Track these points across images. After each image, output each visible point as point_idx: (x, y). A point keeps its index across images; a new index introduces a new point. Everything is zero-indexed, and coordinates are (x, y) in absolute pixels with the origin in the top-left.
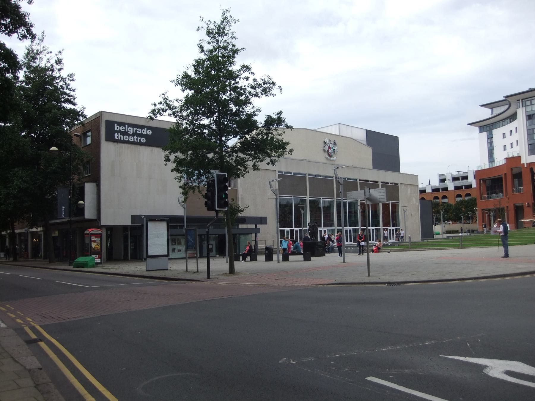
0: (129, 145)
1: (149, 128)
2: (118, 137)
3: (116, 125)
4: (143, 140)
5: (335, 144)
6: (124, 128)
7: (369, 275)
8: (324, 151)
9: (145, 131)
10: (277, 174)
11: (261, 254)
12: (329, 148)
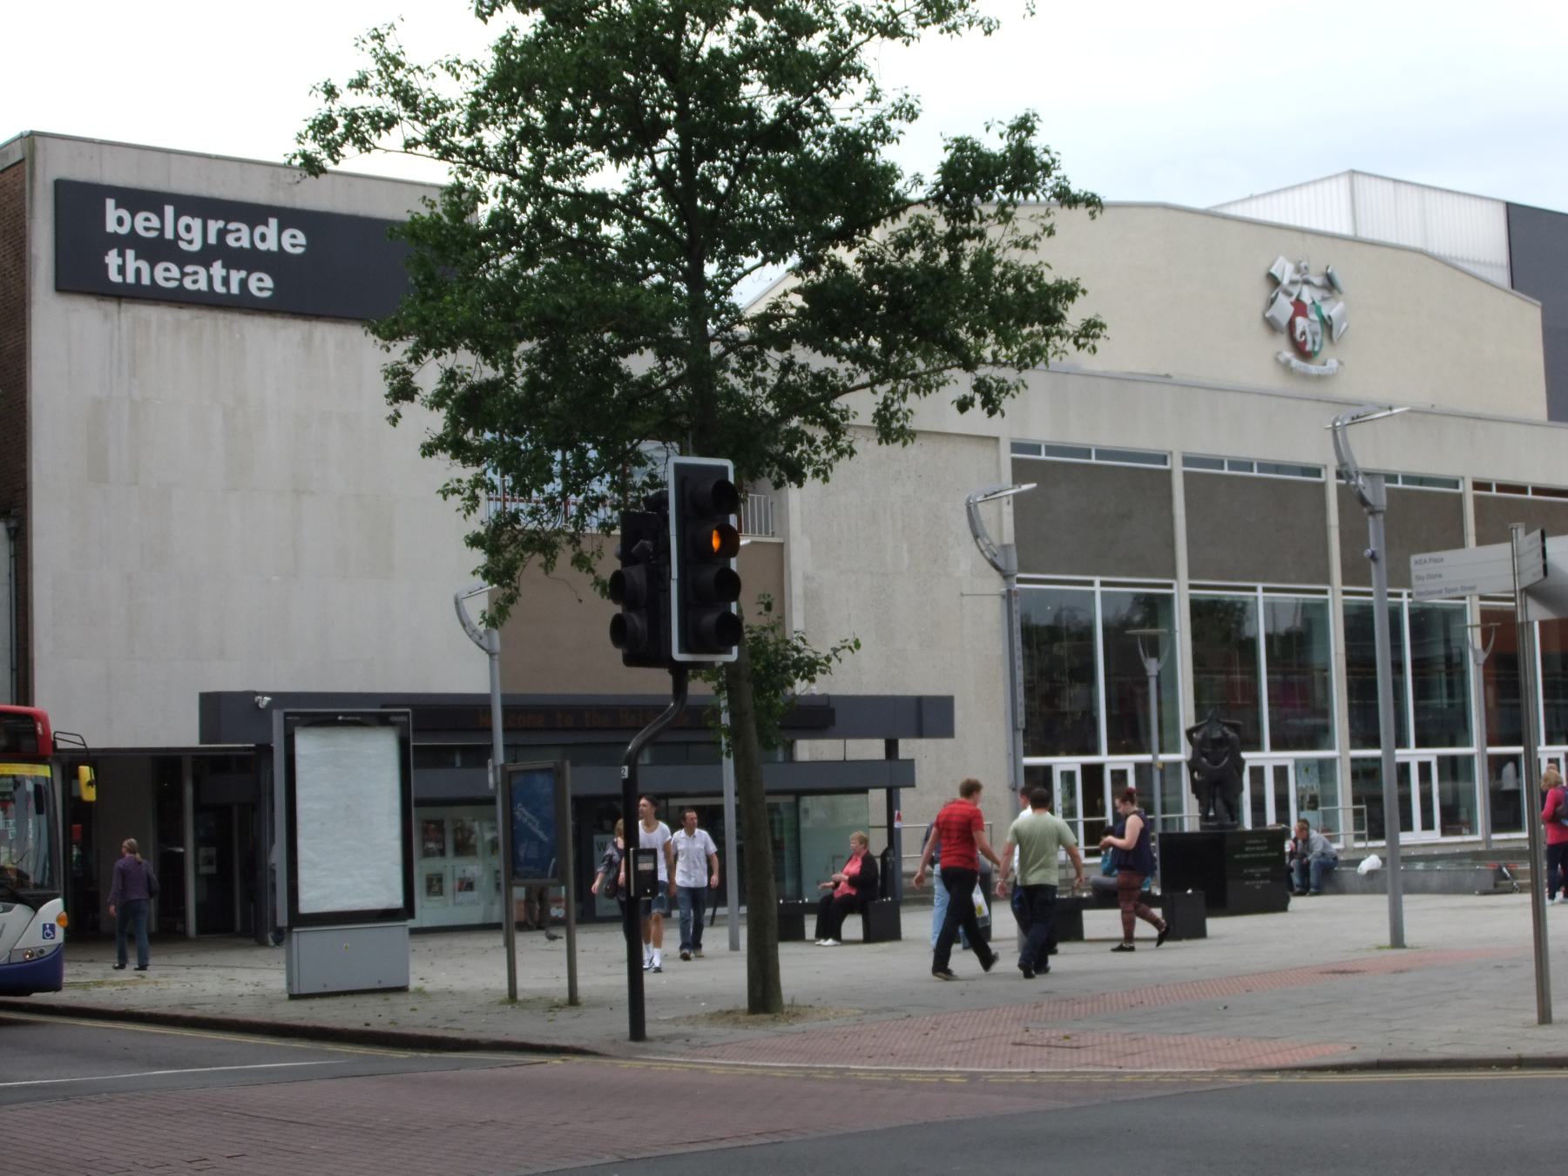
0: (186, 315)
1: (289, 218)
2: (122, 270)
4: (261, 284)
5: (1330, 284)
6: (155, 222)
7: (1545, 1017)
8: (1271, 325)
9: (270, 237)
10: (1007, 456)
12: (1300, 308)
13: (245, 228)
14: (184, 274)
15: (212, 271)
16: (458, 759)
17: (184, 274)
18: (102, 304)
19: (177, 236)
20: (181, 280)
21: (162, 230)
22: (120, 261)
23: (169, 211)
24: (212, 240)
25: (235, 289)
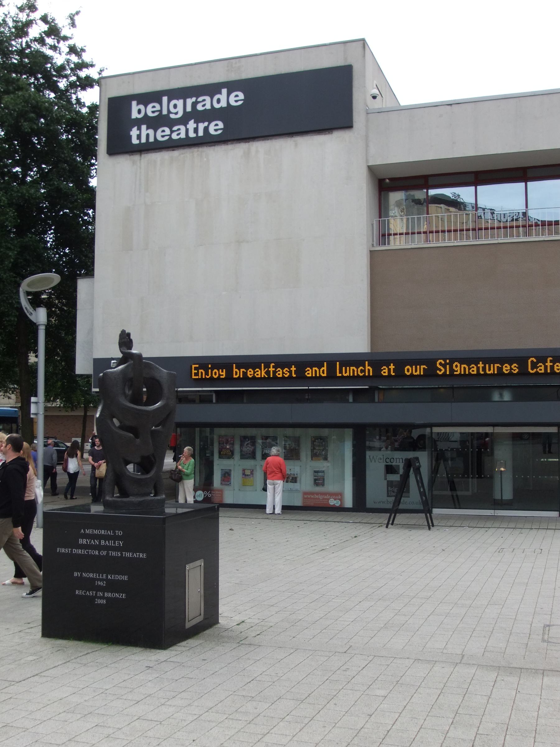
0: (176, 153)
1: (232, 86)
2: (139, 137)
3: (134, 103)
4: (216, 127)
6: (158, 107)
9: (223, 100)
11: (83, 489)
13: (208, 99)
14: (172, 132)
15: (188, 126)
16: (351, 399)
17: (172, 132)
18: (132, 156)
19: (169, 112)
20: (170, 135)
21: (161, 111)
22: (138, 132)
23: (165, 99)
24: (189, 109)
25: (201, 133)
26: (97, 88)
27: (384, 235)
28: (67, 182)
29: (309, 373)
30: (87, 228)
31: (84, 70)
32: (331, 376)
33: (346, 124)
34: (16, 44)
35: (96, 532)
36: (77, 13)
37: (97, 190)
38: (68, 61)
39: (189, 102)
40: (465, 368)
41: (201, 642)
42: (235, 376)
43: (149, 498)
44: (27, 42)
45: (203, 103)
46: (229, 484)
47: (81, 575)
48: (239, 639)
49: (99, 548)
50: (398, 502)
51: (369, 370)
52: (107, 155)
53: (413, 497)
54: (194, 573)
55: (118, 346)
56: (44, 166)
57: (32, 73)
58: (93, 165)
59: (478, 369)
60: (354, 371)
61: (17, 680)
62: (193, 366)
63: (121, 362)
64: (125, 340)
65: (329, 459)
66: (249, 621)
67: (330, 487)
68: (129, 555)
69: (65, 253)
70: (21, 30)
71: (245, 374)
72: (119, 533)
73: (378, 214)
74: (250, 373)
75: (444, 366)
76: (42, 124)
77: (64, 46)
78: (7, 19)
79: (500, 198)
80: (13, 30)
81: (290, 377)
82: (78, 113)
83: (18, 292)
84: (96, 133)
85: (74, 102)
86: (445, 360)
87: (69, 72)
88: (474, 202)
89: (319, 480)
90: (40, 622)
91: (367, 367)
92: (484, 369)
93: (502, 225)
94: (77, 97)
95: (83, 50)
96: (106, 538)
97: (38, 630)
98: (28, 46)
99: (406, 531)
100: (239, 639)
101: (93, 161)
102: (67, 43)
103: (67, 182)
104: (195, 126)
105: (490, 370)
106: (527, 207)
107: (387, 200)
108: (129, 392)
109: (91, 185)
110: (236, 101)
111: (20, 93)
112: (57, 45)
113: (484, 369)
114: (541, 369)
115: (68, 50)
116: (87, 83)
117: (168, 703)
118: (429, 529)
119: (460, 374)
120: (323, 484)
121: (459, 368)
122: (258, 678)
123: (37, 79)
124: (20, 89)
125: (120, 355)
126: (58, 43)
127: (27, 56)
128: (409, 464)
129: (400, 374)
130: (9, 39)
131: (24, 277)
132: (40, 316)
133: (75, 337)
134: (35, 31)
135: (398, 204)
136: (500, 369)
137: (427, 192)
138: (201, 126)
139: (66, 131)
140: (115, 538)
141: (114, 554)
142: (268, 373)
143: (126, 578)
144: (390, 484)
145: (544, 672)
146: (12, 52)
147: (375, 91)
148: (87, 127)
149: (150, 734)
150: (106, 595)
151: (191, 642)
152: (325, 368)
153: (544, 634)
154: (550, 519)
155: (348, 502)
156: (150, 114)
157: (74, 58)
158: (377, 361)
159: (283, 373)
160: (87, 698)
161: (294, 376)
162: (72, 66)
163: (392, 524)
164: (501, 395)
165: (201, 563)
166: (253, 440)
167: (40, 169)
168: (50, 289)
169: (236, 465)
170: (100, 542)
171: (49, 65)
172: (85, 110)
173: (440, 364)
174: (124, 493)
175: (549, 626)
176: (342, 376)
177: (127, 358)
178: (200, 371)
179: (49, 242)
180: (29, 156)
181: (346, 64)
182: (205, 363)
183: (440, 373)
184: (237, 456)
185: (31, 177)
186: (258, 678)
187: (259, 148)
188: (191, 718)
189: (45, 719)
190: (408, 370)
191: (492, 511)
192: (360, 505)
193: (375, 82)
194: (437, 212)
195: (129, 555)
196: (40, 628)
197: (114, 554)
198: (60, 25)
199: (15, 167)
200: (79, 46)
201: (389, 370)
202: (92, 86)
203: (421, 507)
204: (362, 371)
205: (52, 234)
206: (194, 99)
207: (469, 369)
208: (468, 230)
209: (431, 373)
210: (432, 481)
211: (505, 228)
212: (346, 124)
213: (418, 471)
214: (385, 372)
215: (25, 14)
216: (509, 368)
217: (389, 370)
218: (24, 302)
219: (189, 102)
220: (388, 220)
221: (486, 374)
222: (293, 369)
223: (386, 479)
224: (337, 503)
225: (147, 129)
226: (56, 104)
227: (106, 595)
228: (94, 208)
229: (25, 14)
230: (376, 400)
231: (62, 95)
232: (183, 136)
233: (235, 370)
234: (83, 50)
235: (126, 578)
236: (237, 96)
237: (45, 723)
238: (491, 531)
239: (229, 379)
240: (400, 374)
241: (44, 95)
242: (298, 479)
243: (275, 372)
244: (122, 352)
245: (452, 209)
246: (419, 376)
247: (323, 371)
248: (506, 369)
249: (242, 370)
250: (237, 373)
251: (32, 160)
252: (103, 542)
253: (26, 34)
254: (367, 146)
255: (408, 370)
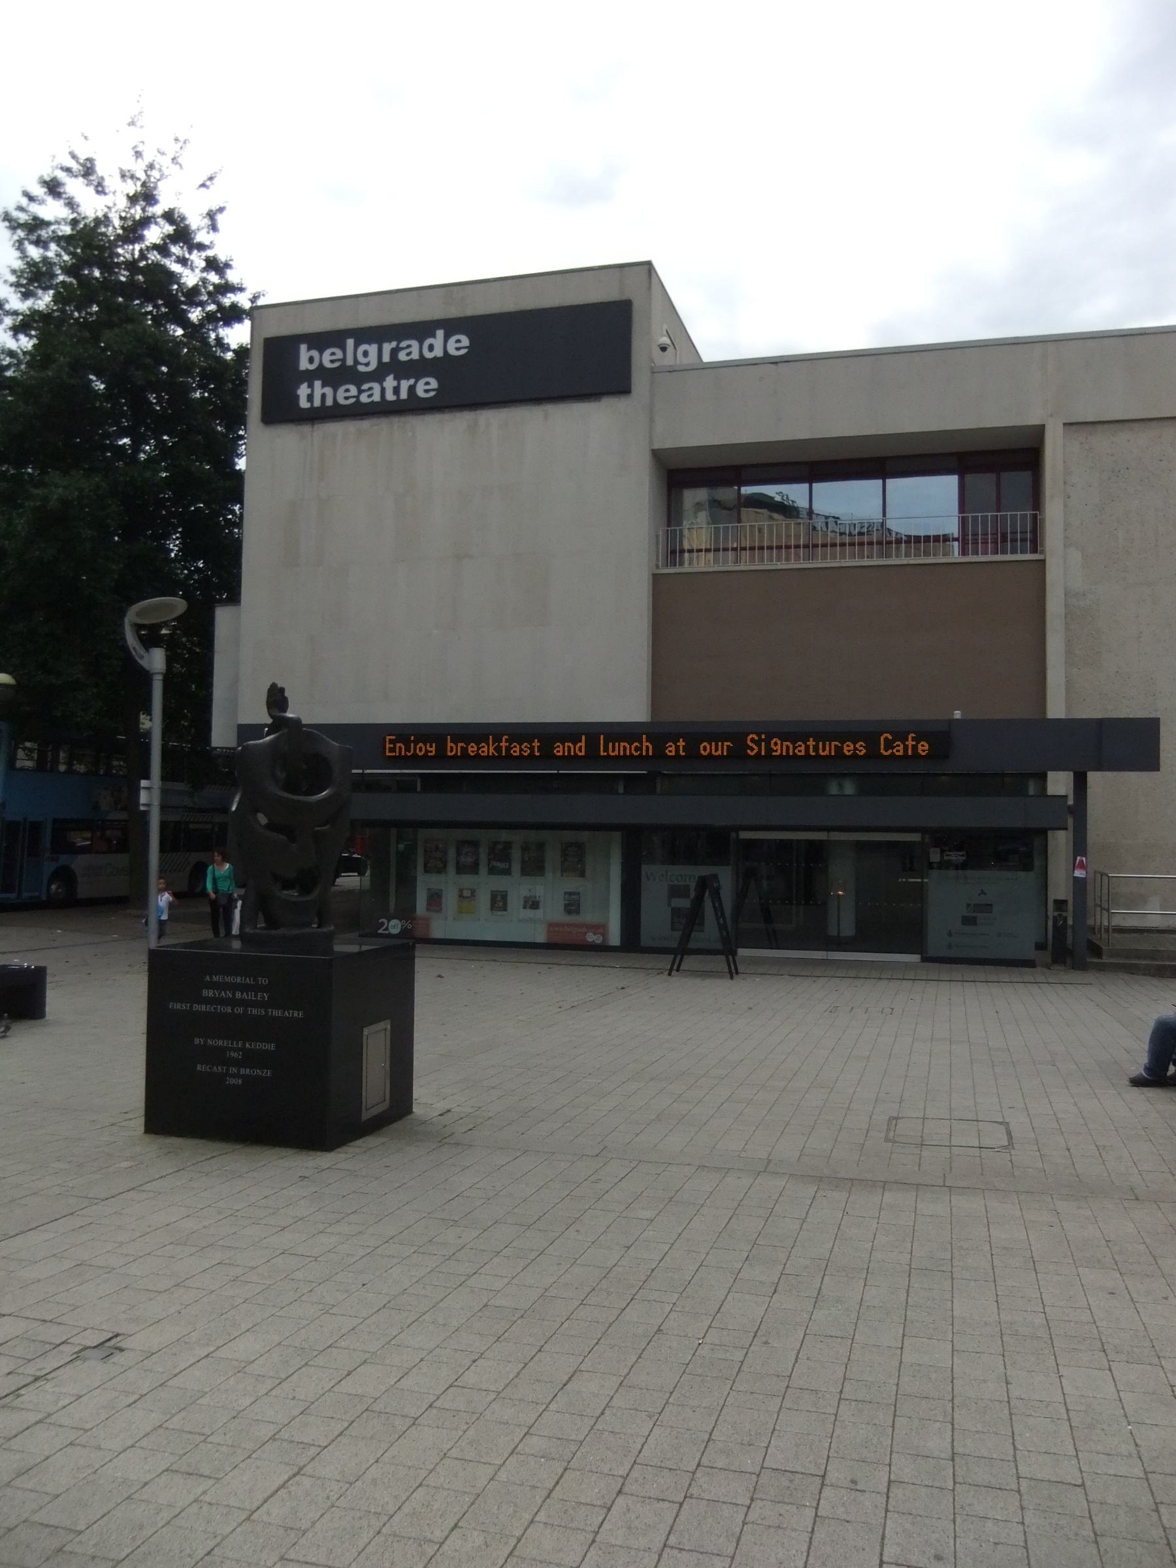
0: (366, 424)
1: (451, 326)
2: (310, 398)
3: (303, 348)
4: (426, 387)
6: (339, 354)
9: (437, 346)
13: (415, 344)
14: (360, 392)
15: (385, 384)
17: (360, 392)
19: (356, 362)
20: (357, 397)
21: (344, 360)
22: (309, 391)
23: (350, 343)
24: (386, 358)
25: (404, 395)
26: (247, 323)
27: (673, 552)
28: (201, 463)
29: (559, 750)
30: (231, 532)
31: (229, 295)
32: (592, 755)
33: (624, 389)
34: (124, 252)
35: (228, 979)
36: (221, 210)
37: (246, 477)
38: (204, 281)
39: (387, 347)
40: (788, 747)
41: (384, 1140)
42: (449, 754)
43: (307, 930)
44: (141, 251)
45: (408, 351)
46: (440, 911)
47: (205, 1042)
48: (443, 1137)
49: (233, 1003)
50: (686, 938)
51: (647, 747)
52: (261, 424)
53: (710, 931)
54: (376, 1042)
55: (266, 709)
56: (165, 438)
57: (149, 298)
58: (242, 437)
59: (807, 747)
60: (625, 748)
61: (102, 1196)
62: (388, 738)
63: (273, 728)
64: (277, 698)
65: (588, 873)
66: (457, 1109)
67: (588, 916)
68: (277, 1013)
69: (197, 568)
70: (133, 231)
71: (464, 750)
72: (263, 981)
73: (665, 519)
74: (472, 749)
75: (758, 743)
76: (163, 373)
77: (197, 259)
78: (110, 215)
79: (847, 501)
80: (120, 232)
81: (532, 755)
82: (221, 360)
83: (122, 625)
84: (245, 392)
85: (213, 343)
86: (759, 735)
87: (205, 298)
88: (807, 506)
89: (572, 905)
90: (142, 1112)
91: (645, 744)
92: (816, 748)
93: (847, 539)
94: (217, 336)
95: (227, 265)
96: (244, 988)
97: (139, 1123)
98: (143, 256)
99: (698, 981)
100: (443, 1137)
101: (241, 433)
102: (204, 254)
103: (201, 463)
104: (395, 383)
105: (824, 750)
106: (884, 514)
107: (680, 501)
108: (282, 775)
109: (238, 468)
110: (458, 349)
111: (130, 327)
112: (187, 256)
113: (816, 748)
114: (899, 750)
115: (203, 264)
116: (233, 315)
117: (328, 1230)
118: (732, 978)
119: (781, 754)
120: (578, 912)
121: (779, 747)
122: (465, 1194)
123: (156, 306)
124: (130, 320)
125: (269, 721)
126: (190, 253)
127: (141, 271)
128: (704, 884)
129: (693, 753)
130: (113, 244)
131: (132, 602)
132: (156, 661)
133: (211, 694)
134: (153, 235)
135: (698, 506)
136: (839, 750)
137: (739, 490)
138: (405, 385)
139: (200, 386)
140: (256, 988)
141: (255, 1011)
142: (498, 749)
143: (272, 1047)
144: (676, 912)
145: (885, 1185)
146: (118, 265)
147: (665, 340)
148: (233, 382)
149: (299, 1275)
150: (242, 1071)
151: (370, 1141)
152: (583, 744)
153: (888, 1130)
154: (907, 966)
155: (615, 939)
156: (328, 365)
157: (213, 278)
158: (657, 733)
159: (521, 750)
160: (206, 1223)
161: (537, 754)
162: (211, 288)
163: (678, 970)
164: (841, 786)
165: (386, 1025)
166: (475, 844)
167: (160, 444)
168: (174, 620)
169: (450, 884)
170: (234, 994)
171: (175, 287)
172: (229, 356)
173: (752, 740)
174: (272, 923)
175: (896, 1118)
176: (609, 755)
177: (279, 723)
178: (398, 745)
179: (172, 550)
180: (142, 423)
181: (624, 298)
182: (406, 733)
183: (752, 754)
184: (451, 869)
185: (145, 452)
186: (465, 1194)
187: (492, 420)
188: (361, 1252)
189: (141, 1254)
190: (705, 749)
191: (824, 953)
192: (633, 943)
193: (665, 327)
194: (753, 519)
195: (277, 1013)
196: (143, 1119)
197: (255, 1011)
198: (194, 227)
199: (122, 438)
200: (222, 258)
201: (677, 748)
202: (240, 320)
203: (719, 946)
204: (637, 749)
205: (177, 538)
206: (394, 344)
207: (795, 748)
208: (797, 547)
209: (738, 753)
210: (738, 909)
211: (852, 544)
212: (624, 389)
213: (716, 895)
214: (671, 750)
215: (138, 208)
216: (852, 747)
217: (677, 748)
218: (131, 640)
219: (387, 347)
220: (681, 531)
221: (818, 756)
222: (536, 744)
223: (669, 905)
224: (598, 939)
225: (323, 386)
226: (185, 345)
227: (242, 1071)
228: (242, 503)
229: (138, 208)
230: (658, 790)
231: (195, 331)
232: (377, 398)
233: (449, 744)
234: (227, 265)
235: (272, 1047)
236: (458, 341)
237: (141, 1260)
238: (822, 981)
239: (441, 758)
240: (693, 753)
241: (166, 330)
242: (541, 905)
243: (508, 749)
244: (272, 716)
245: (776, 516)
246: (721, 757)
247: (580, 748)
248: (848, 748)
249: (460, 745)
250: (453, 749)
251: (147, 428)
252: (238, 995)
253: (141, 238)
254: (652, 420)
255: (705, 748)
